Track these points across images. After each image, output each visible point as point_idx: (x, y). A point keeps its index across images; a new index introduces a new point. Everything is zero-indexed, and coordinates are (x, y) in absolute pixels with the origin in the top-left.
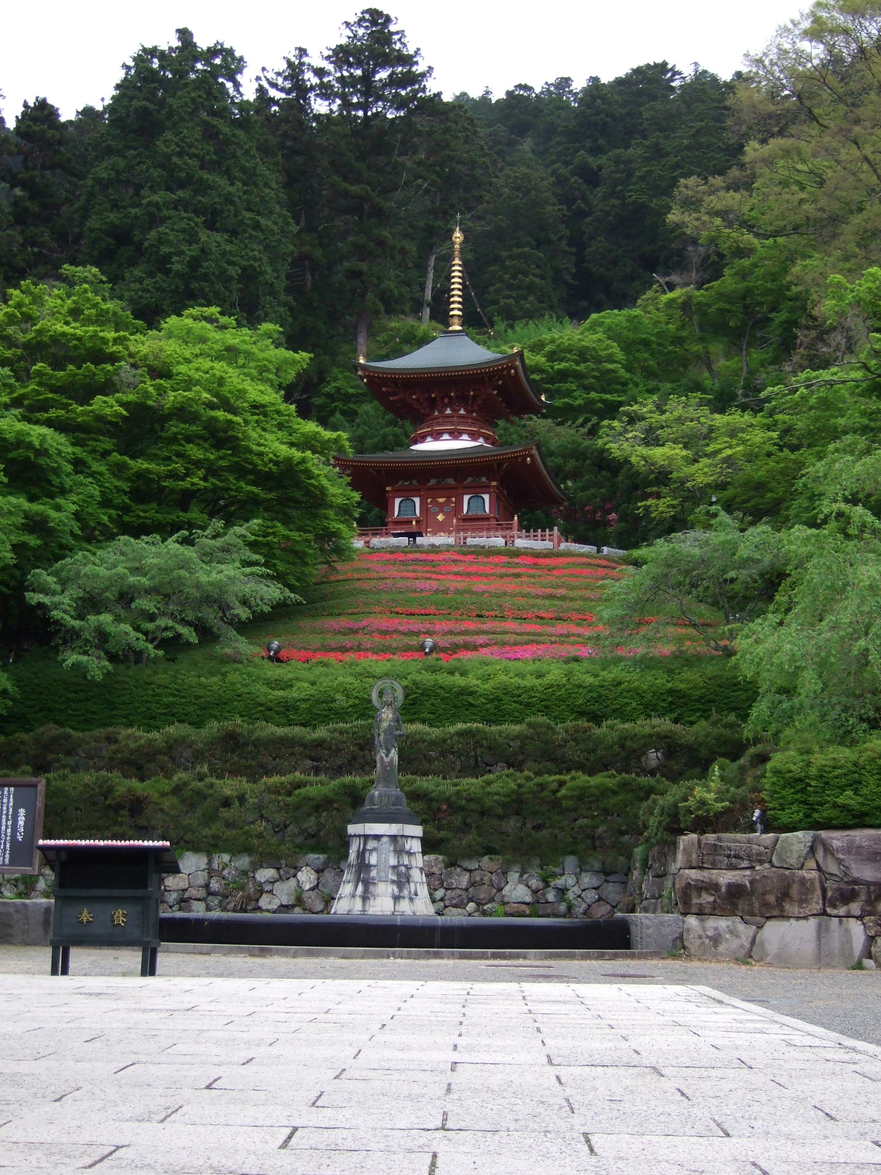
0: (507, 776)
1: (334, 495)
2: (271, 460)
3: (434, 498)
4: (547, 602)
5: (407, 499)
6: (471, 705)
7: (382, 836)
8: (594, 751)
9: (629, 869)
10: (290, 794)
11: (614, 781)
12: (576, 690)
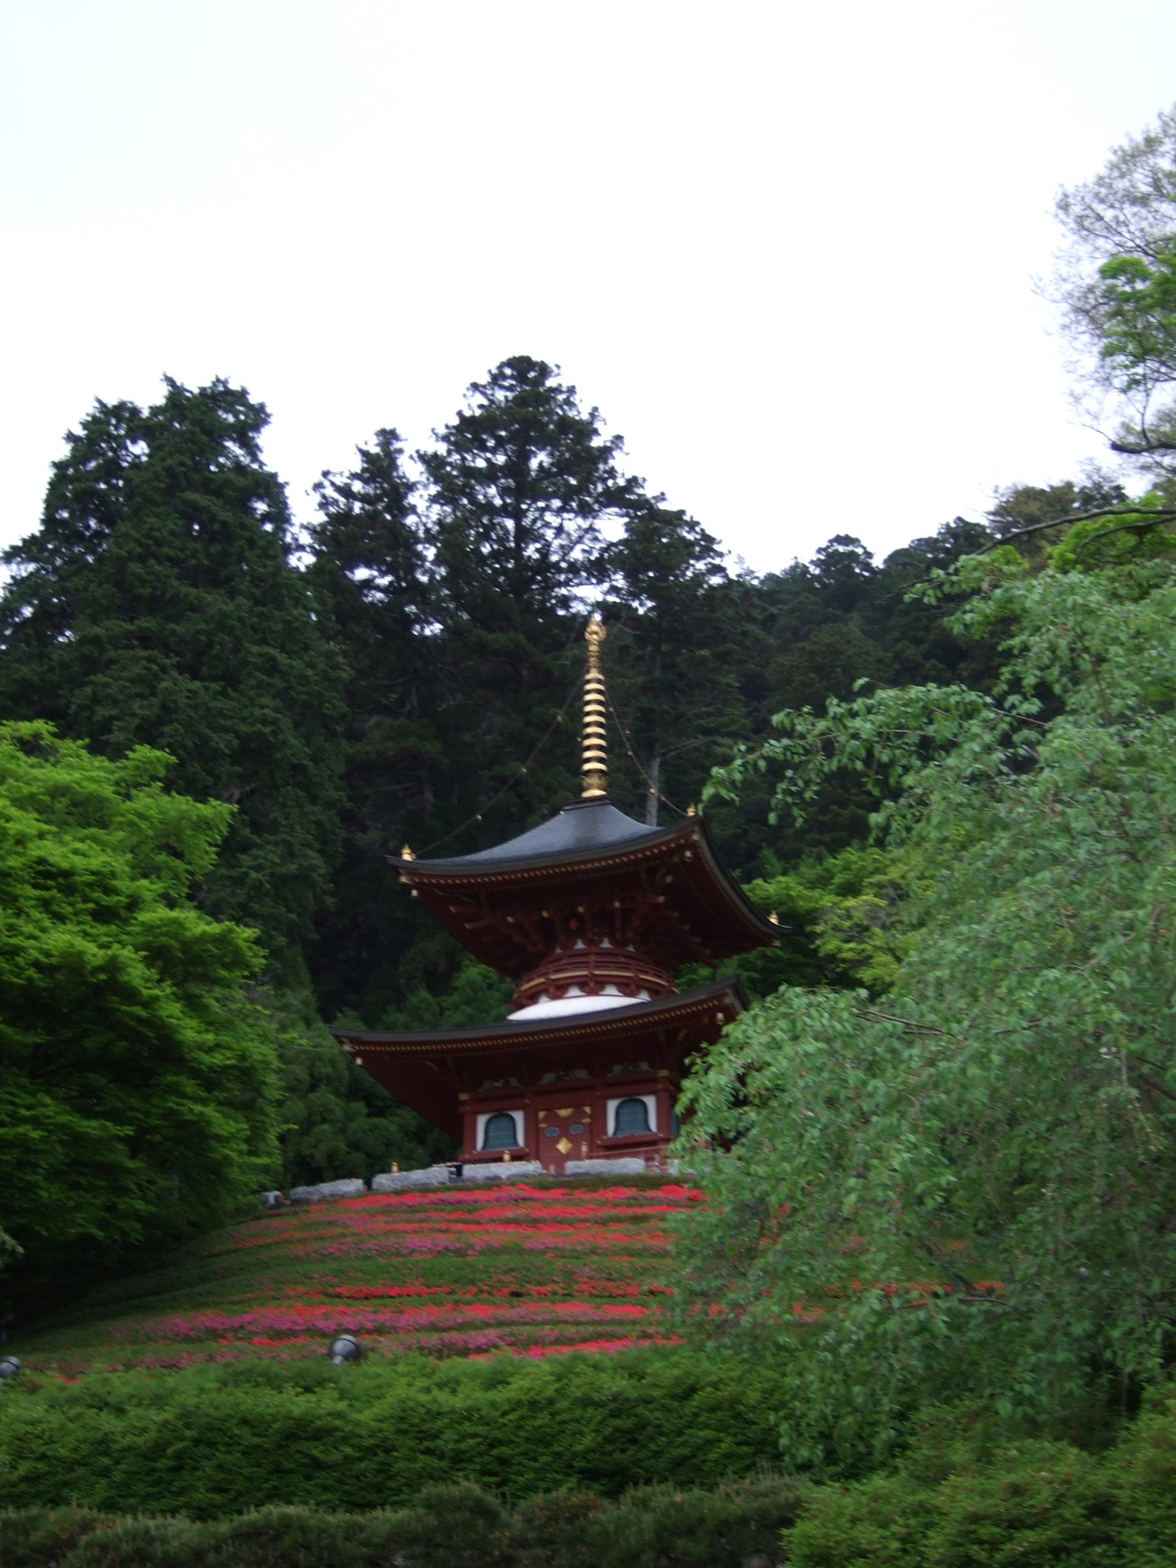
1: (201, 1047)
2: (36, 965)
3: (550, 1110)
6: (318, 1465)
12: (578, 1412)
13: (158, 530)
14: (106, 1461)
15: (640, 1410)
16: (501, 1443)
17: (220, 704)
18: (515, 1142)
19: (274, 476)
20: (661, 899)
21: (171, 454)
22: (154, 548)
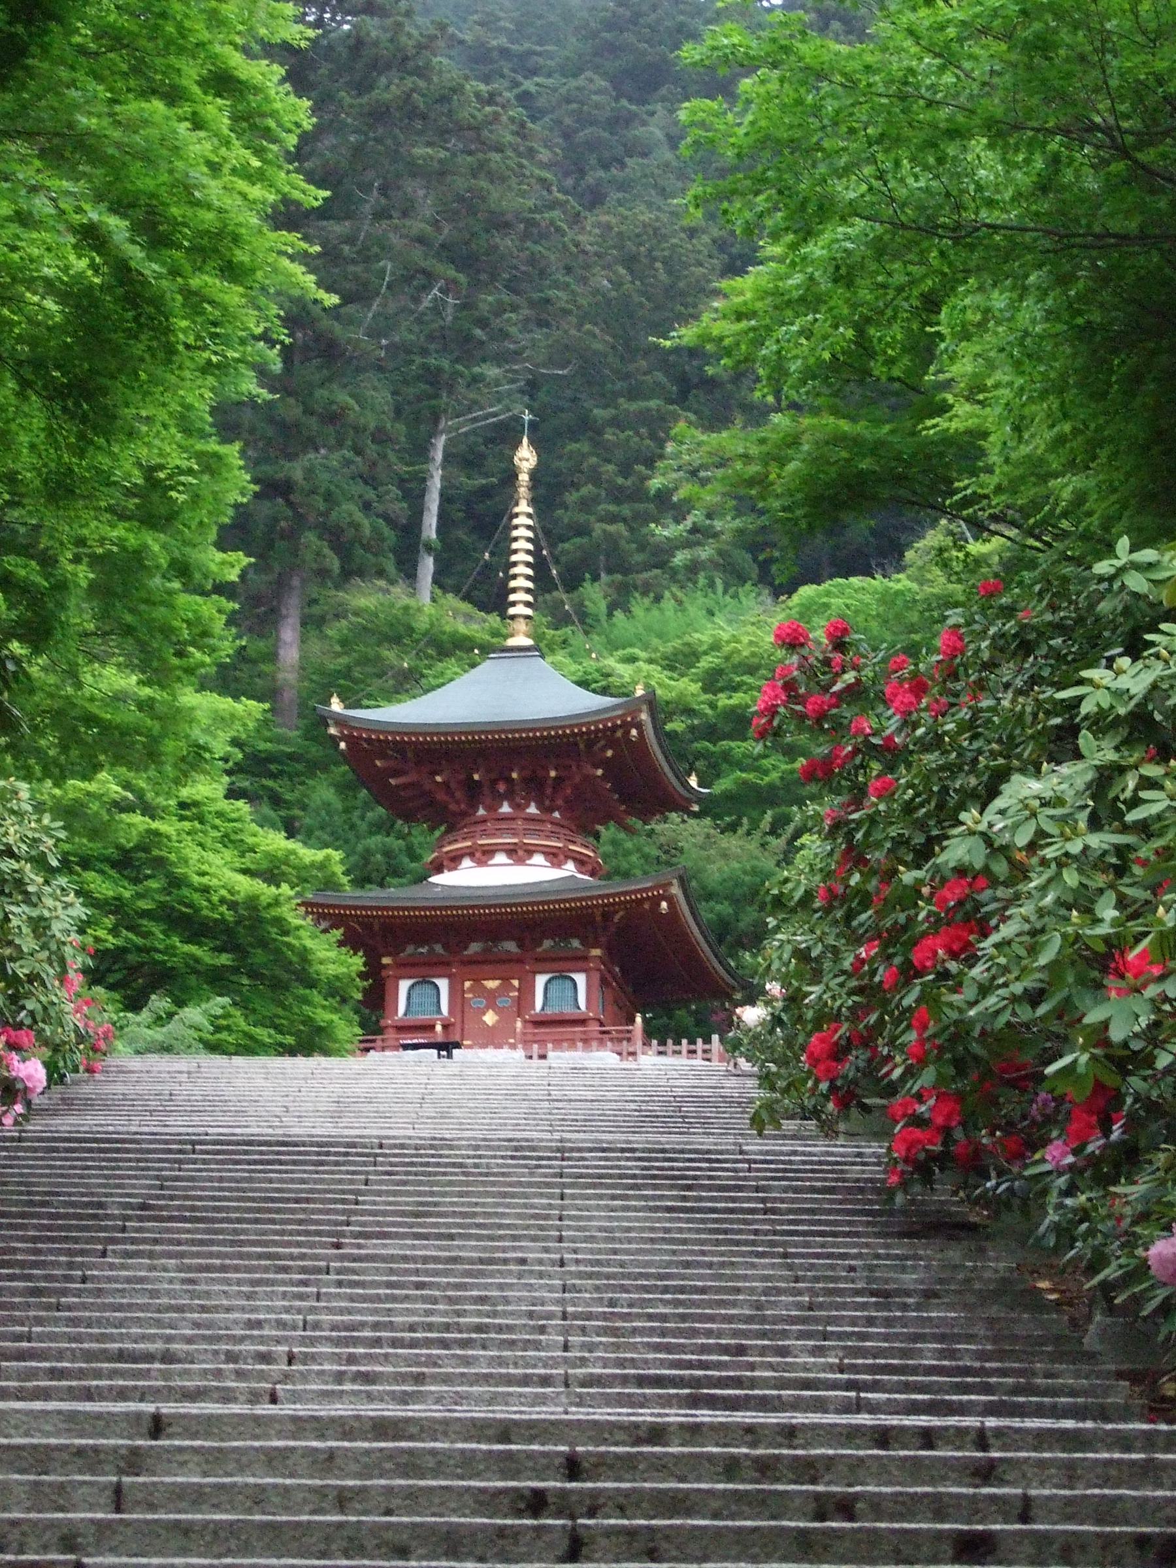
2: (223, 901)
3: (477, 980)
18: (439, 1011)
20: (600, 772)
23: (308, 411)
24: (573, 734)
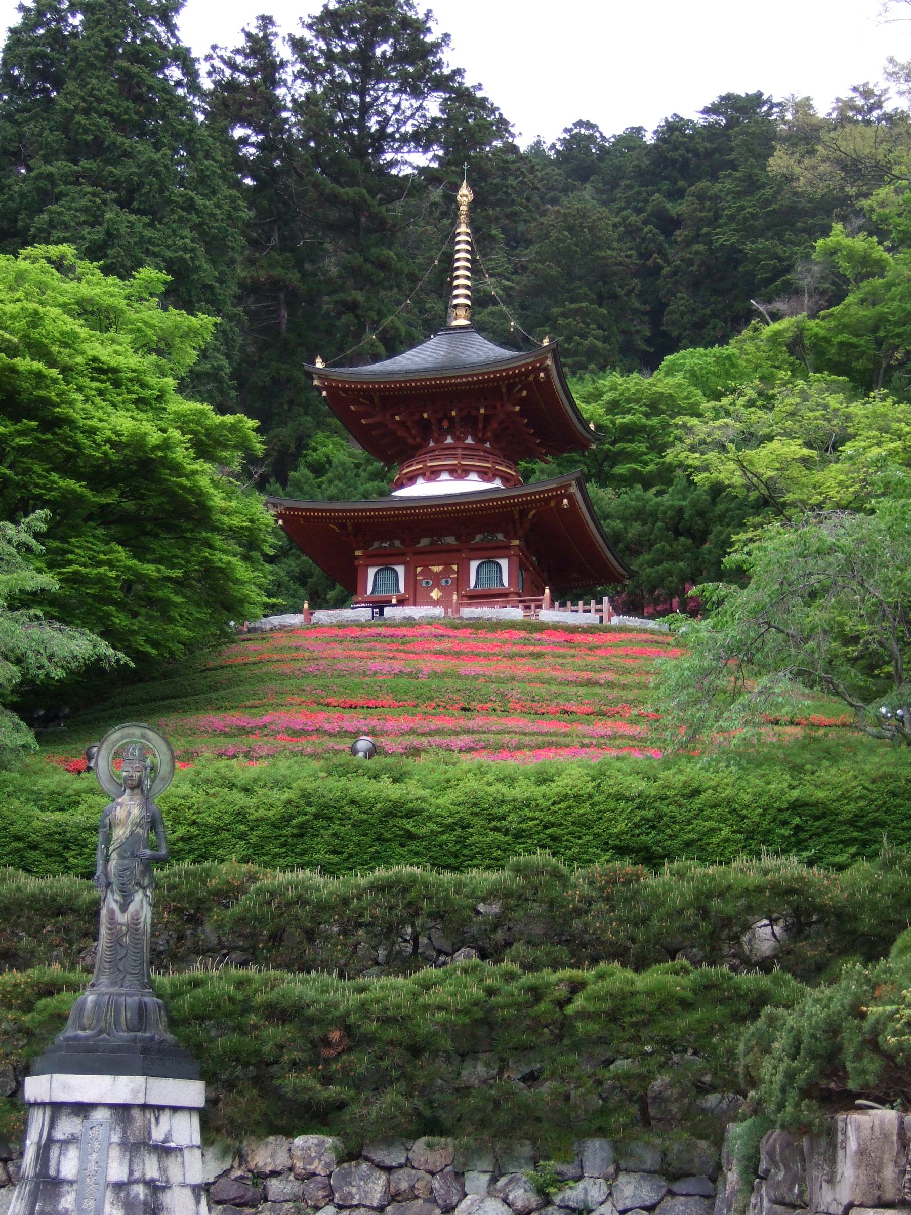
0: (466, 971)
1: (223, 512)
2: (108, 441)
3: (426, 566)
4: (582, 691)
5: (387, 568)
6: (410, 836)
7: (93, 1106)
8: (645, 921)
9: (719, 1167)
10: (28, 1007)
11: (685, 981)
12: (613, 805)
13: (99, 90)
14: (243, 828)
15: (657, 804)
16: (553, 825)
17: (148, 233)
18: (398, 590)
19: (188, 50)
20: (517, 408)
21: (108, 28)
22: (95, 104)
23: (366, 260)
24: (495, 379)
